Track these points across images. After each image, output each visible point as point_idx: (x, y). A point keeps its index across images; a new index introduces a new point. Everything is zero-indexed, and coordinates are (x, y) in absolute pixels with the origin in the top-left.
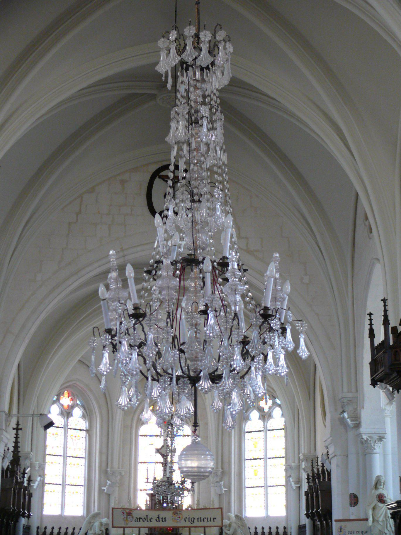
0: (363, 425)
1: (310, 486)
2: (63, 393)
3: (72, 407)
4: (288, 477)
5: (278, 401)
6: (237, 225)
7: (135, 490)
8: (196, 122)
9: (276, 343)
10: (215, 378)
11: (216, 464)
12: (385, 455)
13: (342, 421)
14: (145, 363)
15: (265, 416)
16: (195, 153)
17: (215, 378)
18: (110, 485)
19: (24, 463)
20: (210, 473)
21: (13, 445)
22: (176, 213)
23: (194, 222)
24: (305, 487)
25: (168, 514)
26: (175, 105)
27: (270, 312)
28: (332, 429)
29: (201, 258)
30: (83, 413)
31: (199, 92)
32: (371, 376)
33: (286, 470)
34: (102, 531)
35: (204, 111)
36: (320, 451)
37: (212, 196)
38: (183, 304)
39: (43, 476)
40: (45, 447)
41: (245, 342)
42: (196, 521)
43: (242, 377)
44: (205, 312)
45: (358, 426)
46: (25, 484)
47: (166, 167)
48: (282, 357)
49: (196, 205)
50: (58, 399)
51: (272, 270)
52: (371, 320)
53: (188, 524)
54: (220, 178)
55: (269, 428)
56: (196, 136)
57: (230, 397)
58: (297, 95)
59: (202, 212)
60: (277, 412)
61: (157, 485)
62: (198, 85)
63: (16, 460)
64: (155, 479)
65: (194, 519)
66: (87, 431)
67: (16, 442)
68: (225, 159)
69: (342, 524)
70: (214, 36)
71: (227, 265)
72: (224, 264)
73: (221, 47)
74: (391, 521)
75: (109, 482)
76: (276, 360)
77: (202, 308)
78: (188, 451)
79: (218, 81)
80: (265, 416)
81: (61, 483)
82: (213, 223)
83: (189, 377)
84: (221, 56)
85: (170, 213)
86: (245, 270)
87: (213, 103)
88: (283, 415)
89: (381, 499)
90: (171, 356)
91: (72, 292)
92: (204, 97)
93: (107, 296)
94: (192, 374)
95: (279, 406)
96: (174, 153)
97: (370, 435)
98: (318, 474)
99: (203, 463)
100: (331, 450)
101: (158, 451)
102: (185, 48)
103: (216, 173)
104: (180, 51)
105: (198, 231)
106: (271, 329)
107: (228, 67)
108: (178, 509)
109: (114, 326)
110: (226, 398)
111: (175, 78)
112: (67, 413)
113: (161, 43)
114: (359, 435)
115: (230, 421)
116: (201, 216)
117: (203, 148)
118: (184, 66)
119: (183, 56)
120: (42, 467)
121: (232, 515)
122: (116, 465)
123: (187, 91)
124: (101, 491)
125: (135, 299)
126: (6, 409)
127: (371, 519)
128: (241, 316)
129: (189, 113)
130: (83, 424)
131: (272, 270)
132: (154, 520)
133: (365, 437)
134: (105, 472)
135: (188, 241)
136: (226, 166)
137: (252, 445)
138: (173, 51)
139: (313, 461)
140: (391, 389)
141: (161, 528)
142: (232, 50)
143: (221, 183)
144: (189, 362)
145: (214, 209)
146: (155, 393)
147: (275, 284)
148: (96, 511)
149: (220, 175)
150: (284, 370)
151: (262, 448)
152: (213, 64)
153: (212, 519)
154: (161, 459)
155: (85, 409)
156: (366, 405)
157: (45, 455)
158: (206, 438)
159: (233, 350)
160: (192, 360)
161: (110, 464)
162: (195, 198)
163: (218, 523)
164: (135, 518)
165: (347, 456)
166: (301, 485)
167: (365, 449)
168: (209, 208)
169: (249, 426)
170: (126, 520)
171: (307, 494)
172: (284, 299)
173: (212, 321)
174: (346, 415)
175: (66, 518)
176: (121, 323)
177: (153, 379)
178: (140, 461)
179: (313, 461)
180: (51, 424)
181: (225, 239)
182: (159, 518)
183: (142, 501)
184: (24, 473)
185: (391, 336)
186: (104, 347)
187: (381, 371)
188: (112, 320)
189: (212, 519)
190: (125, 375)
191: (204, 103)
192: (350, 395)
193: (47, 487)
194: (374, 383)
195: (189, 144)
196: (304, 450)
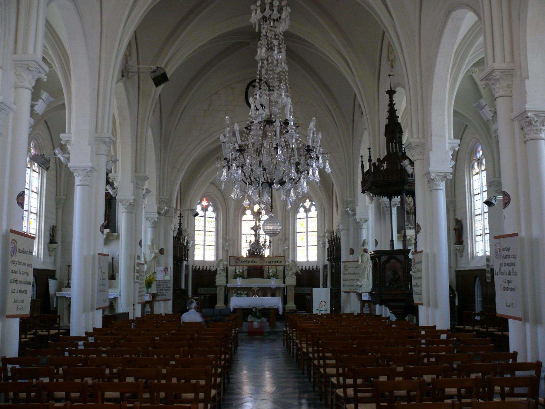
0: (357, 214)
1: (329, 245)
3: (207, 206)
4: (318, 241)
5: (314, 203)
6: (293, 103)
7: (241, 248)
8: (271, 49)
9: (314, 164)
10: (282, 183)
11: (282, 228)
12: (368, 229)
13: (347, 212)
14: (245, 175)
15: (307, 211)
16: (271, 65)
17: (282, 183)
19: (184, 234)
20: (279, 232)
22: (260, 97)
23: (270, 101)
24: (327, 246)
25: (257, 259)
26: (260, 40)
27: (310, 148)
28: (341, 216)
29: (274, 120)
31: (273, 33)
32: (362, 187)
33: (318, 238)
35: (275, 42)
36: (335, 228)
37: (280, 88)
38: (265, 145)
39: (194, 241)
40: (194, 226)
41: (297, 164)
43: (296, 183)
44: (276, 148)
45: (354, 214)
46: (185, 244)
47: (255, 81)
48: (317, 172)
49: (271, 92)
50: (201, 202)
51: (312, 126)
52: (362, 159)
53: (268, 264)
54: (284, 79)
56: (271, 56)
57: (290, 194)
58: (325, 43)
59: (275, 95)
60: (313, 208)
61: (252, 246)
62: (272, 29)
63: (180, 232)
64: (251, 241)
67: (180, 224)
68: (286, 68)
69: (345, 263)
70: (280, 3)
71: (288, 123)
72: (286, 123)
73: (284, 9)
74: (370, 261)
76: (314, 173)
77: (275, 146)
78: (266, 222)
79: (283, 27)
80: (307, 211)
82: (280, 102)
83: (268, 183)
84: (284, 15)
85: (258, 97)
86: (297, 127)
87: (280, 38)
88: (316, 210)
89: (365, 251)
90: (259, 171)
91: (207, 146)
92: (275, 35)
93: (225, 140)
94: (269, 181)
95: (314, 205)
96: (260, 65)
97: (534, 113)
99: (276, 227)
100: (341, 227)
101: (252, 228)
102: (265, 9)
103: (282, 75)
104: (263, 11)
105: (272, 106)
106: (311, 158)
107: (288, 20)
108: (262, 256)
109: (228, 156)
110: (288, 194)
111: (260, 25)
112: (205, 209)
113: (253, 7)
114: (355, 219)
115: (289, 206)
116: (274, 98)
117: (275, 62)
118: (265, 19)
119: (265, 13)
120: (193, 236)
121: (290, 260)
122: (231, 235)
123: (266, 33)
124: (223, 249)
125: (239, 142)
126: (175, 207)
127: (360, 261)
128: (296, 150)
129: (268, 44)
130: (214, 215)
131: (312, 126)
132: (250, 262)
133: (358, 220)
134: (225, 239)
135: (267, 111)
136: (287, 72)
137: (300, 225)
138: (259, 11)
139: (331, 233)
140: (372, 195)
141: (254, 266)
142: (290, 11)
143: (285, 81)
144: (268, 175)
145: (281, 95)
146: (250, 192)
147: (313, 134)
148: (221, 258)
149: (284, 77)
150: (318, 179)
151: (306, 241)
152: (280, 18)
154: (253, 232)
156: (359, 204)
157: (195, 230)
158: (276, 215)
159: (291, 167)
160: (270, 174)
161: (227, 234)
162: (270, 89)
163: (283, 263)
167: (358, 227)
168: (278, 94)
169: (299, 216)
170: (236, 262)
171: (328, 249)
172: (318, 142)
173: (280, 152)
174: (348, 209)
175: (206, 261)
176: (232, 154)
177: (249, 184)
179: (331, 233)
180: (197, 214)
181: (287, 111)
183: (244, 253)
184: (184, 239)
185: (372, 167)
186: (223, 167)
187: (366, 187)
188: (227, 154)
190: (235, 182)
191: (275, 39)
192: (351, 199)
193: (196, 247)
194: (363, 192)
195: (267, 60)
196: (327, 227)
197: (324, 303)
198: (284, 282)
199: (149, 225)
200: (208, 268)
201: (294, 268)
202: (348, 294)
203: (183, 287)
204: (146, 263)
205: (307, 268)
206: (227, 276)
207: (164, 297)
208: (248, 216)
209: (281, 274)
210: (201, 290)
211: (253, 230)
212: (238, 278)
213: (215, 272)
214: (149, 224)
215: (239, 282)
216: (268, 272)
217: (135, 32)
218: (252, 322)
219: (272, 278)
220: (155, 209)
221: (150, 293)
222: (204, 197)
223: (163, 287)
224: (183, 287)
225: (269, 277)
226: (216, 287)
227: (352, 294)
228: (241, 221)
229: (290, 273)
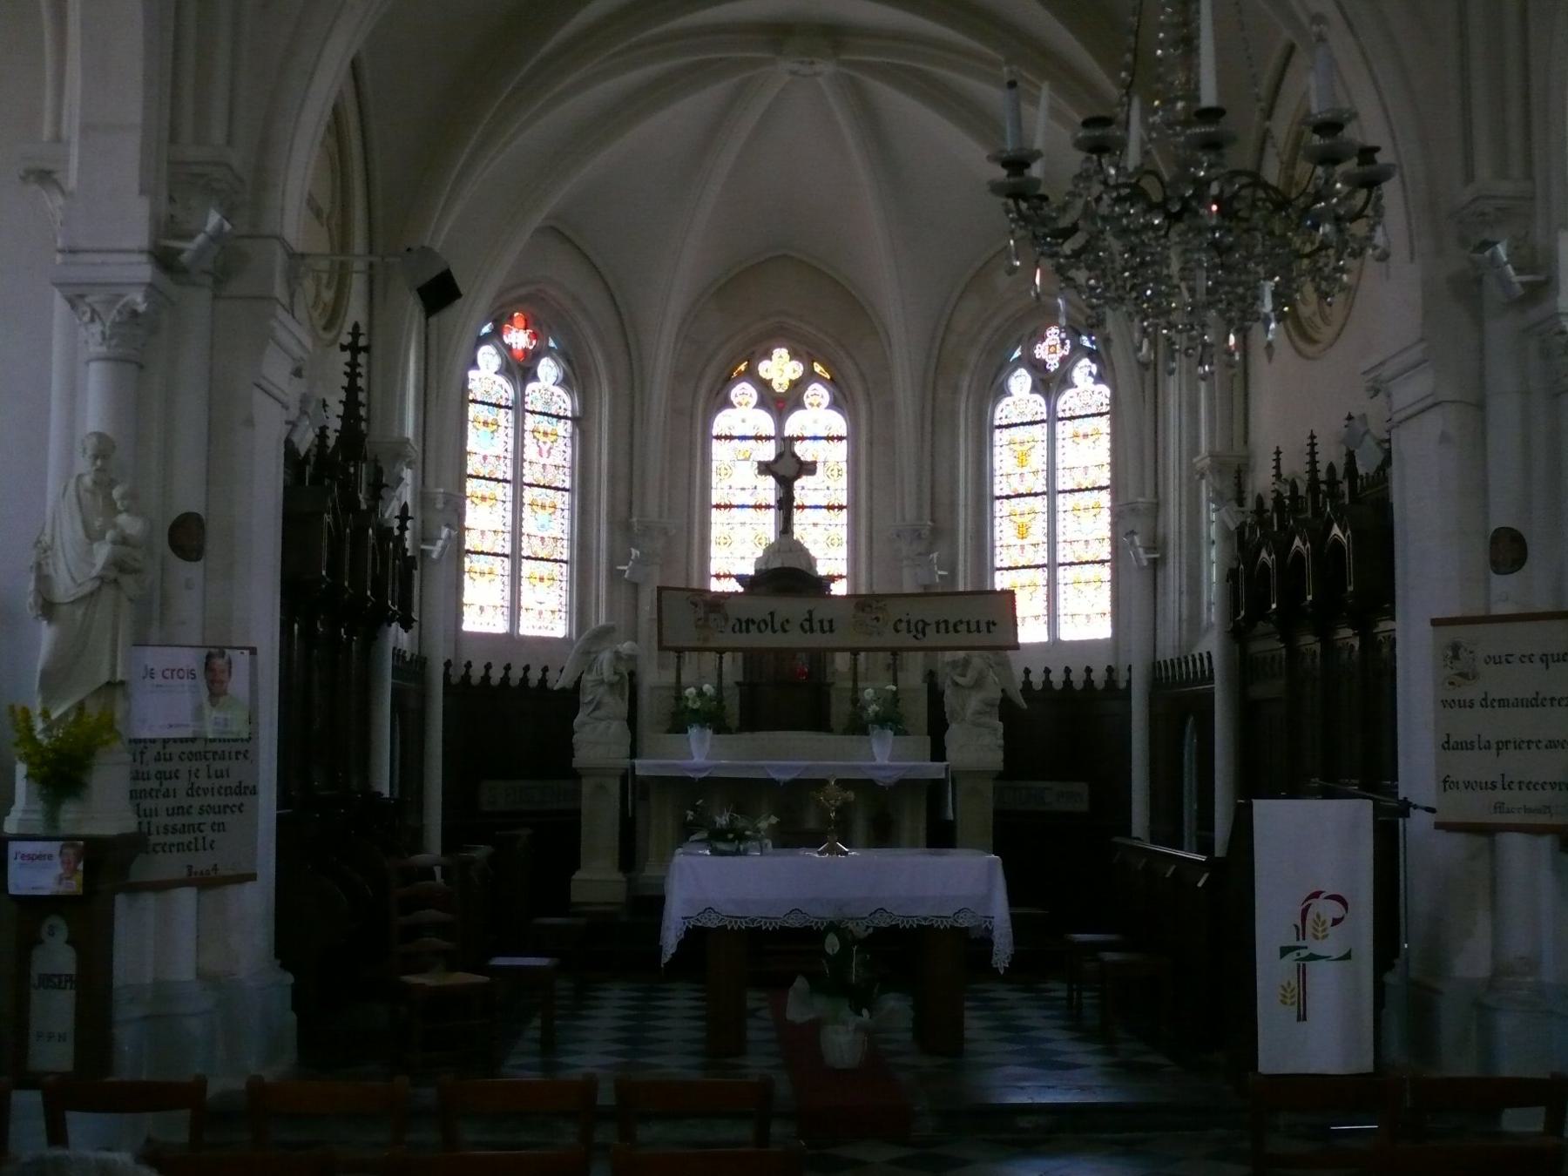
2: (511, 317)
3: (533, 357)
15: (1050, 383)
18: (637, 561)
21: (343, 395)
30: (565, 373)
34: (622, 677)
39: (460, 529)
40: (462, 455)
42: (931, 630)
50: (497, 333)
55: (1060, 415)
60: (1083, 371)
65: (926, 624)
66: (574, 420)
75: (635, 552)
80: (1050, 383)
81: (508, 551)
98: (1332, 482)
101: (765, 468)
112: (520, 370)
124: (614, 576)
130: (564, 402)
137: (1014, 460)
148: (603, 621)
153: (983, 627)
154: (767, 489)
155: (569, 362)
161: (637, 499)
164: (732, 622)
165: (1481, 406)
166: (1164, 558)
169: (1005, 411)
178: (715, 500)
182: (810, 620)
189: (983, 627)
197: (1335, 909)
198: (938, 753)
199: (96, 348)
200: (535, 676)
201: (992, 677)
202: (1482, 841)
203: (383, 784)
204: (48, 608)
205: (1057, 679)
206: (632, 721)
207: (202, 862)
208: (742, 414)
209: (918, 710)
210: (496, 795)
211: (770, 481)
212: (693, 732)
213: (570, 699)
214: (93, 339)
215: (700, 752)
216: (855, 701)
217: (355, 66)
218: (815, 1026)
219: (875, 731)
220: (132, 223)
221: (69, 839)
222: (518, 303)
223: (192, 791)
224: (383, 784)
225: (858, 727)
226: (576, 776)
227: (1515, 847)
228: (707, 438)
229: (974, 702)
